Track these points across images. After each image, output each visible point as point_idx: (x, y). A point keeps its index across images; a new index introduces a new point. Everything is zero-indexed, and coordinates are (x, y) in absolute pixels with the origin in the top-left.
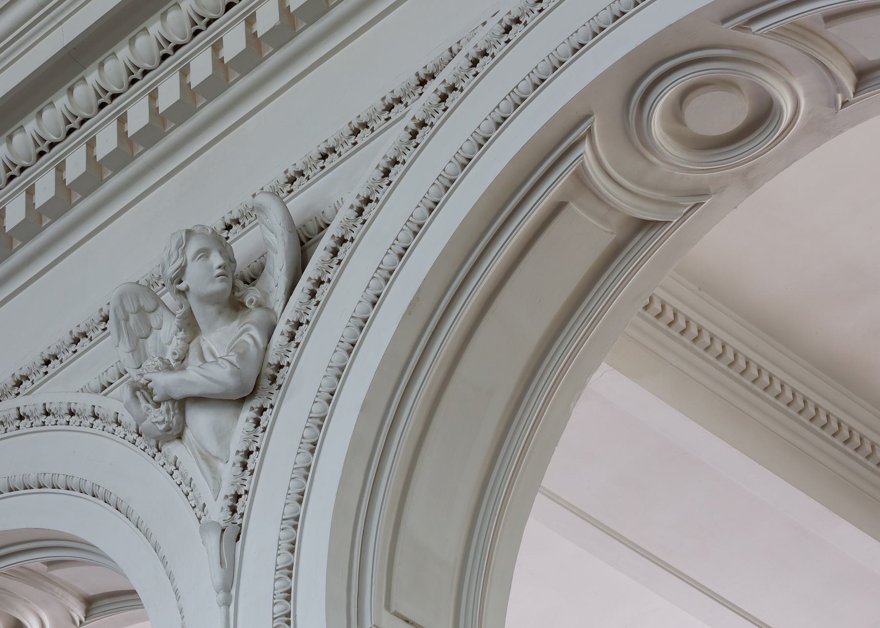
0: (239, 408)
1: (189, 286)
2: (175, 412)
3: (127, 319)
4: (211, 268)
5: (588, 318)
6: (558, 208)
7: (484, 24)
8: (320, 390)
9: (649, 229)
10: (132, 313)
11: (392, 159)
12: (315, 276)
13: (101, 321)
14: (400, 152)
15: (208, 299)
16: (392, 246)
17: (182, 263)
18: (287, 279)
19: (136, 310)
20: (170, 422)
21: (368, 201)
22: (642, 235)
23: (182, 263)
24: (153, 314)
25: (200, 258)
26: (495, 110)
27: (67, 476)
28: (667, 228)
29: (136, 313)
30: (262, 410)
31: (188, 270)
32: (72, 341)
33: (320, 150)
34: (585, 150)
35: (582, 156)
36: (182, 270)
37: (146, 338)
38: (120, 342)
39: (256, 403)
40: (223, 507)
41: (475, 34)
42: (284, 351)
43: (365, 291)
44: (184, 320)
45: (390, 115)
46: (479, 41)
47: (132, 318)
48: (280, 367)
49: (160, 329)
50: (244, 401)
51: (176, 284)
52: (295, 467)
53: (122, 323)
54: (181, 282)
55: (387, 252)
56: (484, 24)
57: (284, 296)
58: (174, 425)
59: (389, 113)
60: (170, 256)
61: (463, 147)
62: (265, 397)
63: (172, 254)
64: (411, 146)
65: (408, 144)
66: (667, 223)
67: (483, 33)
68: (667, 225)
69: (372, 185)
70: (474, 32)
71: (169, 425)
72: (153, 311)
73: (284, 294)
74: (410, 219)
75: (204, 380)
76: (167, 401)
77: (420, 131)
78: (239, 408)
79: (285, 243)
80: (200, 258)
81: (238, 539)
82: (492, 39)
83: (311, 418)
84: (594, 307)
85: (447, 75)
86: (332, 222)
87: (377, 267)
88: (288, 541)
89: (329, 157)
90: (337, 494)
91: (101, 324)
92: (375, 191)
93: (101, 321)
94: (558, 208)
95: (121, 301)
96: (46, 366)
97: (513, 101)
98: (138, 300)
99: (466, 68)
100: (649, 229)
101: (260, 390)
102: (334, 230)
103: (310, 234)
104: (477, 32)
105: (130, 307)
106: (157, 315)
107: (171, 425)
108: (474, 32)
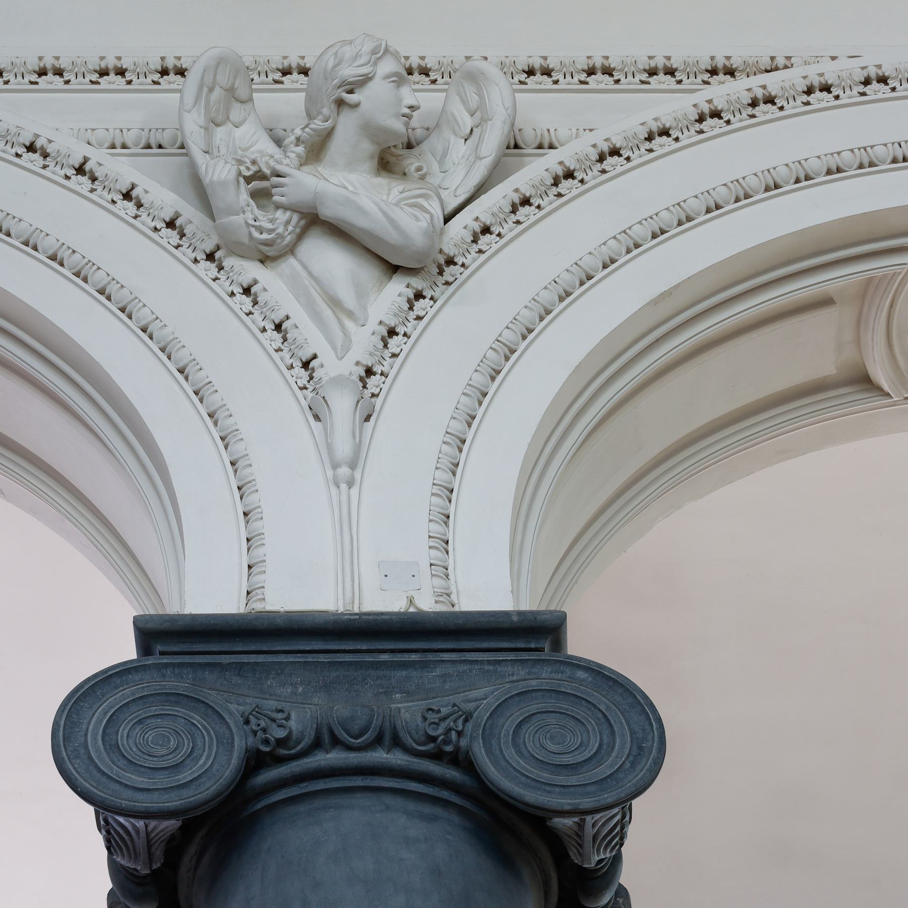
0: (385, 274)
1: (361, 105)
2: (295, 230)
3: (211, 90)
4: (400, 101)
5: (748, 439)
6: (826, 302)
7: (833, 58)
8: (516, 317)
9: (861, 390)
10: (221, 87)
11: (60, 68)
12: (527, 192)
13: (95, 71)
14: (686, 69)
15: (370, 130)
16: (649, 219)
17: (370, 73)
18: (486, 173)
19: (228, 87)
20: (281, 236)
21: (671, 72)
22: (857, 389)
23: (370, 73)
24: (239, 104)
25: (393, 82)
26: (834, 155)
27: (8, 214)
28: (883, 400)
29: (225, 90)
30: (419, 296)
31: (371, 85)
32: (37, 69)
33: (530, 62)
34: (12, 238)
35: (906, 266)
36: (366, 80)
37: (218, 125)
38: (194, 109)
39: (417, 283)
40: (352, 373)
41: (818, 62)
42: (693, 71)
43: (600, 246)
44: (318, 136)
45: (100, 80)
46: (831, 73)
47: (217, 93)
48: (450, 262)
49: (237, 127)
50: (395, 272)
51: (344, 91)
52: (469, 383)
53: (205, 90)
54: (351, 92)
55: (641, 221)
56: (833, 58)
57: (472, 189)
58: (283, 244)
59: (99, 78)
60: (357, 56)
61: (776, 169)
62: (428, 283)
63: (361, 55)
64: (693, 128)
65: (271, 71)
66: (888, 395)
67: (843, 64)
68: (885, 397)
69: (631, 139)
70: (817, 59)
71: (276, 239)
72: (242, 102)
73: (474, 187)
74: (681, 203)
75: (380, 215)
76: (294, 211)
77: (599, 74)
78: (385, 274)
79: (503, 132)
80: (393, 82)
81: (368, 418)
82: (847, 80)
83: (498, 341)
84: (761, 431)
85: (774, 82)
86: (561, 145)
87: (623, 230)
88: (451, 460)
89: (130, 203)
90: (530, 444)
91: (93, 74)
92: (624, 72)
93: (95, 71)
94: (826, 302)
95: (218, 65)
96: (160, 75)
97: (149, 138)
98: (235, 78)
99: (91, 67)
100: (861, 390)
101: (425, 272)
102: (565, 155)
103: (523, 142)
104: (822, 62)
105: (224, 79)
106: (244, 109)
107: (279, 241)
108: (817, 59)
